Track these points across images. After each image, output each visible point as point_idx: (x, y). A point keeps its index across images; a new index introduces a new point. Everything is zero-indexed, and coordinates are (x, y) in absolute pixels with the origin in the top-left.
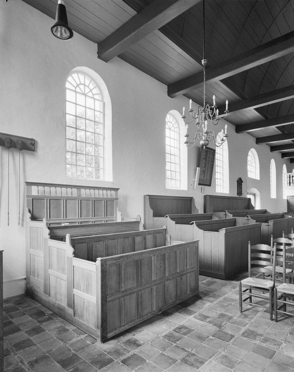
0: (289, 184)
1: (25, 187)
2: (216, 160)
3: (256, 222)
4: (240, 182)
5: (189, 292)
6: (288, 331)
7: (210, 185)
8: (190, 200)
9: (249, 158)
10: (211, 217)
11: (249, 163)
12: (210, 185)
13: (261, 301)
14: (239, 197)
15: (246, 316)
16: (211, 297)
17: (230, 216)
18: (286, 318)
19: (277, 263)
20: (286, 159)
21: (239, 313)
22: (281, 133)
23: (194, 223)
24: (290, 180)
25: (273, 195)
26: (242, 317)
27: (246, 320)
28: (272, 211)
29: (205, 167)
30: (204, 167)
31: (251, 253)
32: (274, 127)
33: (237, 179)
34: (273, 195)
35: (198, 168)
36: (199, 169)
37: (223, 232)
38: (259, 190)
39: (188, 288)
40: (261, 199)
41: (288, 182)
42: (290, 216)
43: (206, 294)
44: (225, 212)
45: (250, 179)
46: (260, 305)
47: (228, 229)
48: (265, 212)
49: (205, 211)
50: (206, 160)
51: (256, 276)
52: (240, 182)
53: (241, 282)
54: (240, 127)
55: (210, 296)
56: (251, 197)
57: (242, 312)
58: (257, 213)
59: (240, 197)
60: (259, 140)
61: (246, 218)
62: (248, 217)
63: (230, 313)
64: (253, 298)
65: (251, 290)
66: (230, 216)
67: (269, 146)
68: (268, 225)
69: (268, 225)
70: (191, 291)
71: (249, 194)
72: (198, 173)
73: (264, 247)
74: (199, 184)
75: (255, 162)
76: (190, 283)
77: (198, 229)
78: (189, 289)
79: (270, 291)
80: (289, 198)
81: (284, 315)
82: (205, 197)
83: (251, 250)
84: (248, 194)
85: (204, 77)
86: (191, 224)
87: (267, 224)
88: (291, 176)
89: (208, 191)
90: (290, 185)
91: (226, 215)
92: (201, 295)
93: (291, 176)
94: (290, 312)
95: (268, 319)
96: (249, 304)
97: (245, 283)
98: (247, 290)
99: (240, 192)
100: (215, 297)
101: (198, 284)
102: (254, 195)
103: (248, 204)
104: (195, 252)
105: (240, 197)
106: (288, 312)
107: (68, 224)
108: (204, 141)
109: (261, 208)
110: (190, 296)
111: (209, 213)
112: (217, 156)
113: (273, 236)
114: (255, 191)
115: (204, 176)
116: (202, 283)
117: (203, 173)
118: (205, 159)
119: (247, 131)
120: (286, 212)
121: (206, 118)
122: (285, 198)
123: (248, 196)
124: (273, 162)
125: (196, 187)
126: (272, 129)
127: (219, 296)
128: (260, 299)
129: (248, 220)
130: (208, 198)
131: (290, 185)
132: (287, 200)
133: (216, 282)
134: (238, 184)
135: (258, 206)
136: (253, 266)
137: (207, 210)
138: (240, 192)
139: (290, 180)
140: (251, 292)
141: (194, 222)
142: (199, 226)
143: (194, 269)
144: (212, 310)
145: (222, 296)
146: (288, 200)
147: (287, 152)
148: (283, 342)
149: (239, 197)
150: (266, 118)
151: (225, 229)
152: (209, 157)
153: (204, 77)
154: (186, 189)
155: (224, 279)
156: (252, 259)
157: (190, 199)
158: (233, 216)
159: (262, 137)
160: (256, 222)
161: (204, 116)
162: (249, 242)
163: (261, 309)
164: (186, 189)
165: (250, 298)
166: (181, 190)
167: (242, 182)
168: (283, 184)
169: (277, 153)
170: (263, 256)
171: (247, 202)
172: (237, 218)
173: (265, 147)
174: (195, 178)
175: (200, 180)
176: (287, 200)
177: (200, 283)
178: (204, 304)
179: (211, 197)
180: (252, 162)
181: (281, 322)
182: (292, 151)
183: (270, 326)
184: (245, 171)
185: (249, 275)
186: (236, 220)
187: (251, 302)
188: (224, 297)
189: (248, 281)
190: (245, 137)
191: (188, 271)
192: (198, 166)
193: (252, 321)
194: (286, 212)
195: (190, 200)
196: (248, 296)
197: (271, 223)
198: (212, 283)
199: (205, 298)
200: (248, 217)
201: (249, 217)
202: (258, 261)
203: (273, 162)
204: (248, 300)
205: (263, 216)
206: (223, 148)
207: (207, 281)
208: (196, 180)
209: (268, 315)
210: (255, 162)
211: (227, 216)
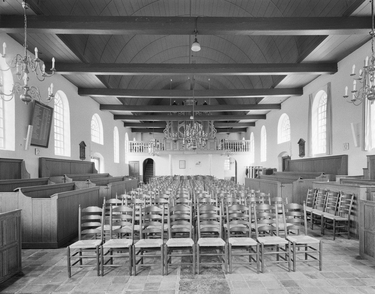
0: (130, 151)
1: (3, 81)
2: (55, 120)
3: (96, 185)
4: (83, 146)
5: (6, 273)
6: (112, 281)
7: (47, 147)
8: (20, 163)
9: (93, 123)
10: (46, 183)
11: (93, 127)
12: (47, 147)
13: (92, 261)
14: (81, 160)
15: (74, 280)
16: (37, 270)
17: (70, 181)
18: (112, 270)
19: (106, 222)
20: (128, 128)
21: (68, 278)
22: (122, 104)
23: (20, 190)
24: (131, 147)
25: (117, 160)
26: (71, 281)
27: (74, 284)
28: (114, 174)
29: (40, 125)
30: (38, 126)
31: (82, 216)
32: (115, 97)
33: (80, 142)
34: (117, 160)
35: (29, 126)
36: (31, 128)
37: (55, 198)
38: (102, 154)
39: (5, 268)
40: (105, 163)
41: (130, 148)
42: (130, 179)
43: (31, 269)
44: (64, 176)
45: (93, 142)
46: (91, 264)
47: (60, 194)
48: (108, 175)
49: (40, 176)
50: (41, 118)
51: (92, 238)
52: (83, 146)
53: (69, 248)
54: (83, 90)
55: (36, 270)
56: (96, 162)
57: (70, 277)
58: (95, 177)
59: (83, 160)
60: (103, 107)
61: (86, 182)
62: (88, 181)
63: (57, 282)
64: (83, 260)
65: (81, 253)
66: (70, 181)
67: (113, 114)
68: (107, 188)
69: (107, 188)
70: (9, 270)
71: (93, 158)
72: (30, 132)
73: (93, 209)
74: (32, 145)
75: (99, 127)
76: (9, 262)
77: (25, 196)
78: (5, 268)
79: (130, 249)
80: (130, 163)
81: (111, 267)
82: (40, 159)
83: (81, 213)
84: (91, 158)
85: (26, 23)
86: (16, 191)
87: (106, 187)
88: (132, 144)
89: (44, 153)
90: (131, 152)
91: (65, 179)
92: (24, 272)
93: (132, 144)
94: (116, 264)
95: (95, 276)
96: (80, 267)
97: (73, 247)
98: (77, 253)
99: (83, 156)
100: (43, 269)
101: (20, 260)
102: (99, 159)
103: (92, 169)
104: (16, 224)
105: (83, 160)
106: (146, 264)
107: (360, 186)
108: (25, 95)
109: (105, 170)
110: (8, 277)
111: (44, 178)
112: (55, 115)
113: (105, 198)
114: (99, 155)
115: (39, 136)
116: (29, 258)
117: (36, 132)
118: (41, 117)
119: (90, 95)
120: (128, 175)
121: (27, 70)
122: (127, 162)
123: (92, 160)
124: (116, 129)
125: (28, 148)
126: (113, 99)
127: (48, 267)
128: (92, 259)
129: (88, 184)
130: (44, 161)
131: (131, 152)
132: (129, 165)
133: (47, 253)
134: (80, 147)
135: (101, 169)
136: (83, 228)
137: (43, 175)
138: (83, 156)
139: (131, 147)
140: (81, 254)
141: (19, 188)
142: (26, 193)
143: (14, 244)
144: (35, 285)
145: (50, 267)
146: (130, 165)
147: (128, 122)
148: (105, 292)
149: (81, 160)
150: (108, 87)
151: (57, 194)
152: (45, 116)
153: (26, 23)
154: (13, 149)
155: (57, 247)
156: (83, 222)
157: (19, 161)
158: (73, 180)
159: (106, 104)
160: (96, 185)
161: (25, 68)
162: (80, 205)
163: (91, 268)
164: (13, 149)
165: (81, 260)
166: (5, 151)
167: (85, 146)
168: (126, 150)
169: (120, 122)
170: (93, 217)
171: (90, 166)
172: (76, 182)
173: (108, 114)
174: (26, 137)
175: (33, 139)
176: (129, 165)
177: (23, 259)
178: (27, 281)
179: (47, 159)
180: (96, 127)
181: (107, 275)
182: (131, 122)
183: (96, 282)
184: (89, 135)
185: (141, 237)
186: (74, 184)
187: (81, 264)
188: (53, 266)
189: (76, 246)
190: (86, 100)
191: (5, 248)
192: (31, 123)
193: (80, 282)
194: (128, 175)
195: (20, 163)
196: (78, 259)
197: (109, 186)
198: (40, 255)
199: (29, 274)
200: (88, 181)
201: (89, 181)
202: (89, 223)
203: (116, 129)
204: (79, 262)
205: (106, 180)
206: (63, 107)
207: (35, 255)
208: (28, 140)
209: (96, 272)
210: (99, 127)
211: (66, 181)
